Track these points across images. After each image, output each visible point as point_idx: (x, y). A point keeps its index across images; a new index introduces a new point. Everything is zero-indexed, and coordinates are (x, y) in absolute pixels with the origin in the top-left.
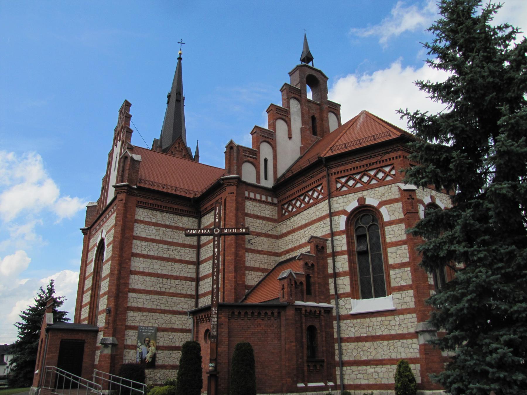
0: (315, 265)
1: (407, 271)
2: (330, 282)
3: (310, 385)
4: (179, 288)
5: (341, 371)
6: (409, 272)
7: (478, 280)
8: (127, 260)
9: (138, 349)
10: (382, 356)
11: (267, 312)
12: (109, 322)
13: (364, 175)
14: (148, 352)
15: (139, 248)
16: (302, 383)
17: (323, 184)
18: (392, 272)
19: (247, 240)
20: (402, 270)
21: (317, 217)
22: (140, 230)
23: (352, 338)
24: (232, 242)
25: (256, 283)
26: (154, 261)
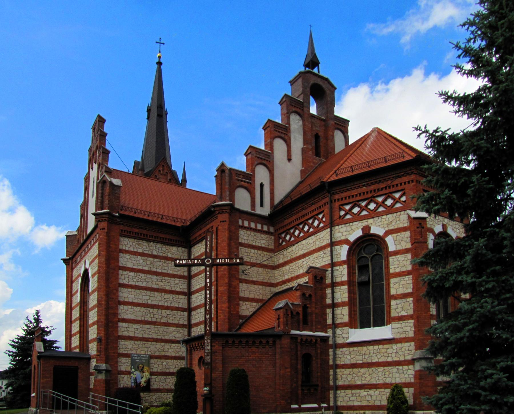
0: (313, 295)
1: (409, 302)
2: (327, 312)
3: (303, 406)
4: (171, 318)
6: (411, 302)
7: (482, 311)
8: (115, 291)
9: (132, 375)
10: (376, 381)
11: (262, 340)
14: (142, 378)
15: (127, 279)
17: (325, 211)
19: (241, 271)
20: (404, 300)
21: (317, 247)
22: (126, 260)
23: (347, 364)
24: (225, 272)
25: (251, 313)
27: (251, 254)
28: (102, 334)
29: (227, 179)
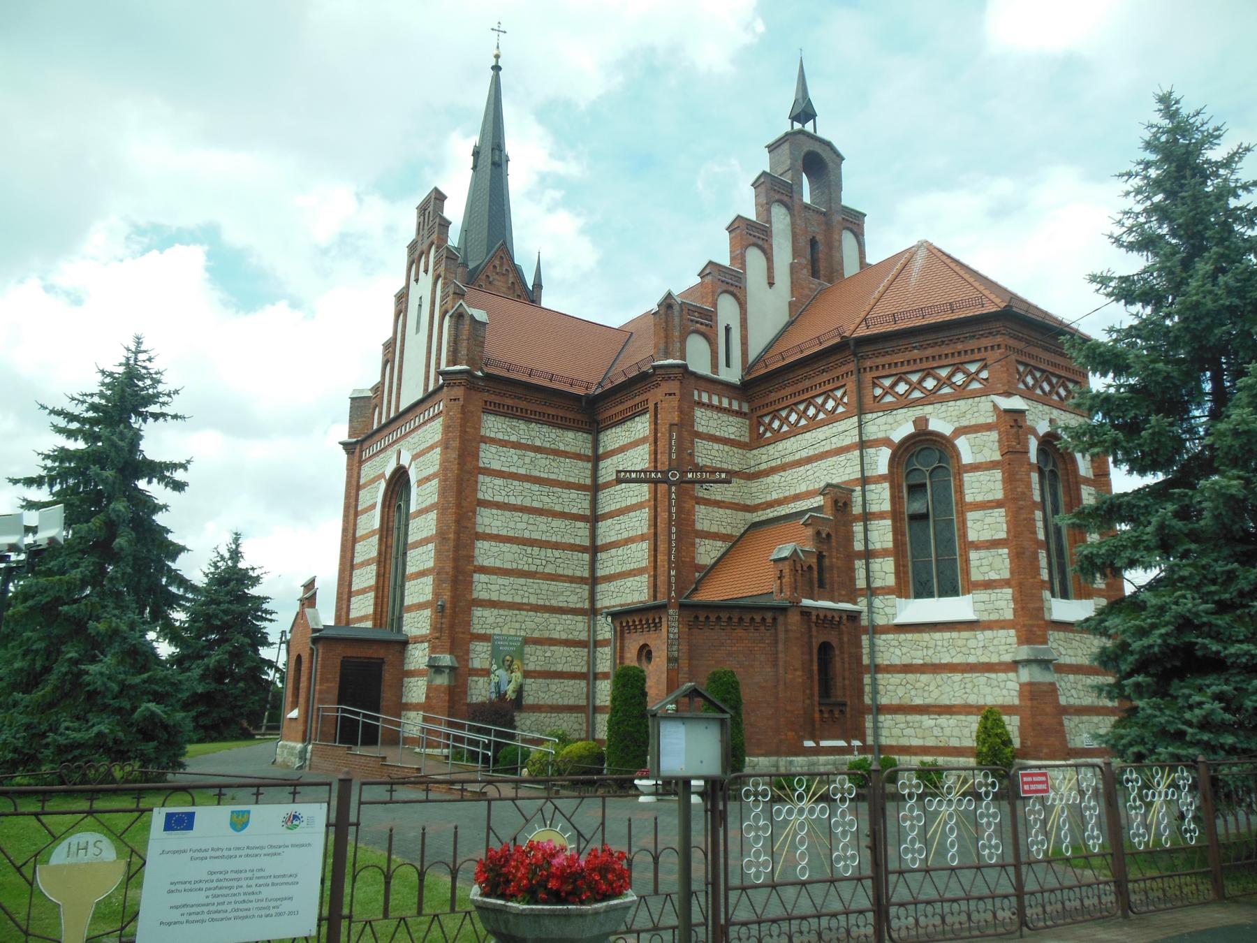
0: (833, 535)
3: (824, 743)
5: (876, 722)
7: (1179, 609)
9: (492, 676)
12: (441, 628)
13: (928, 375)
14: (510, 682)
15: (490, 490)
16: (810, 739)
18: (973, 555)
20: (993, 552)
22: (490, 455)
23: (896, 665)
25: (713, 561)
26: (517, 514)
27: (714, 453)
28: (447, 596)
29: (677, 320)
